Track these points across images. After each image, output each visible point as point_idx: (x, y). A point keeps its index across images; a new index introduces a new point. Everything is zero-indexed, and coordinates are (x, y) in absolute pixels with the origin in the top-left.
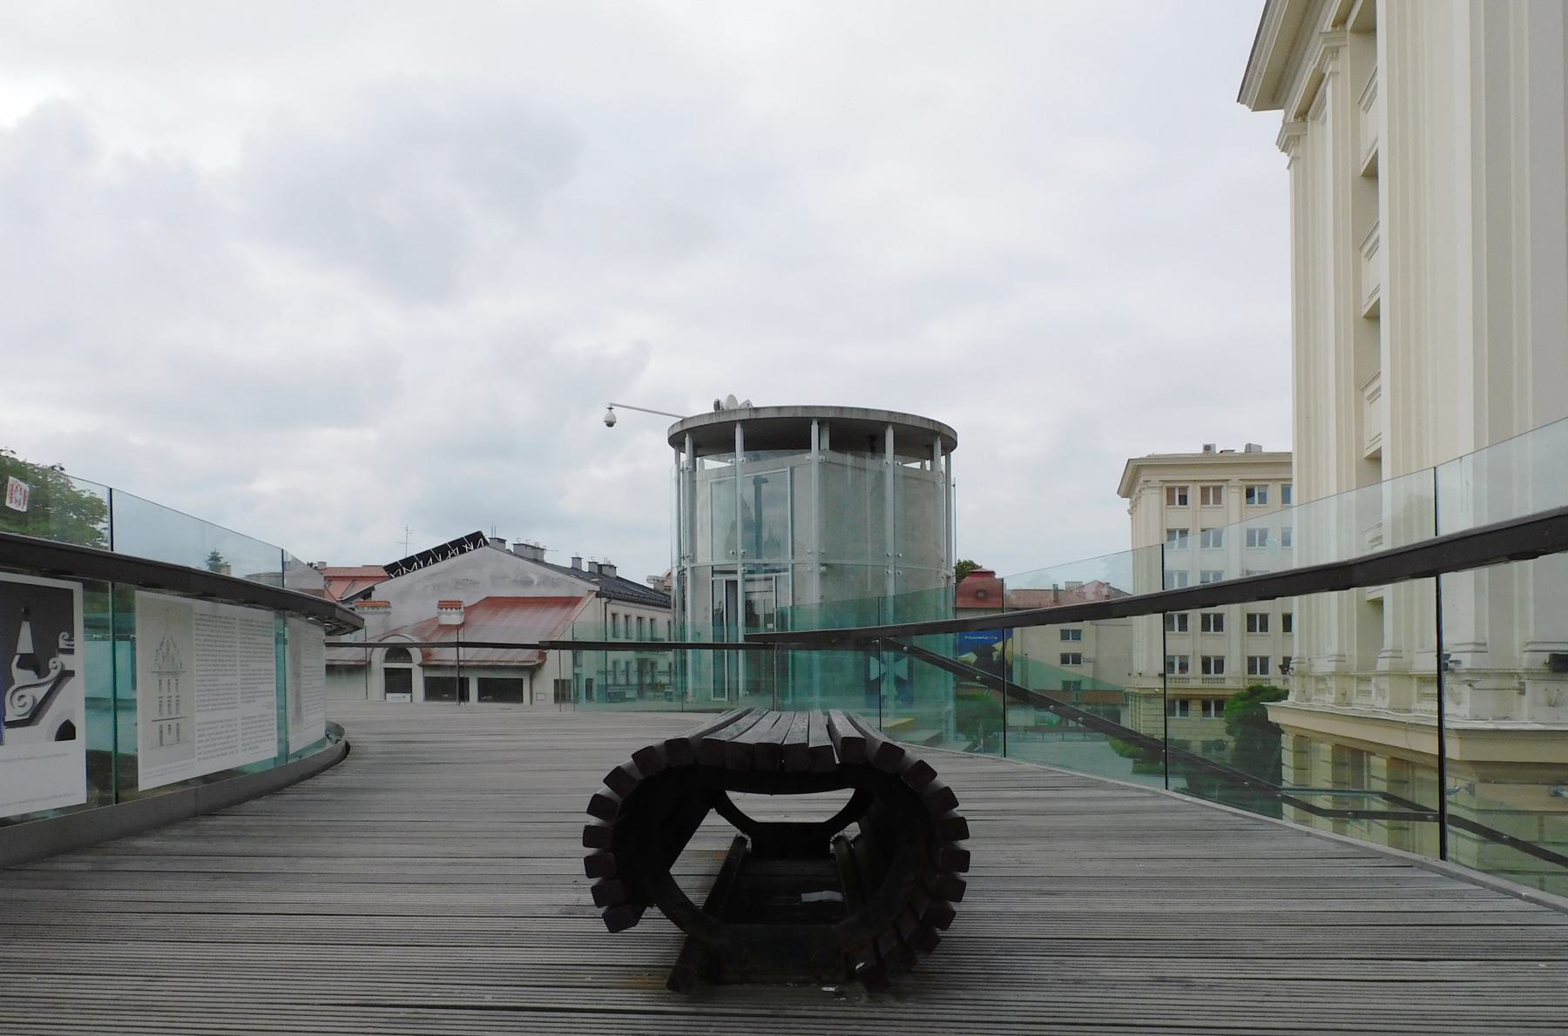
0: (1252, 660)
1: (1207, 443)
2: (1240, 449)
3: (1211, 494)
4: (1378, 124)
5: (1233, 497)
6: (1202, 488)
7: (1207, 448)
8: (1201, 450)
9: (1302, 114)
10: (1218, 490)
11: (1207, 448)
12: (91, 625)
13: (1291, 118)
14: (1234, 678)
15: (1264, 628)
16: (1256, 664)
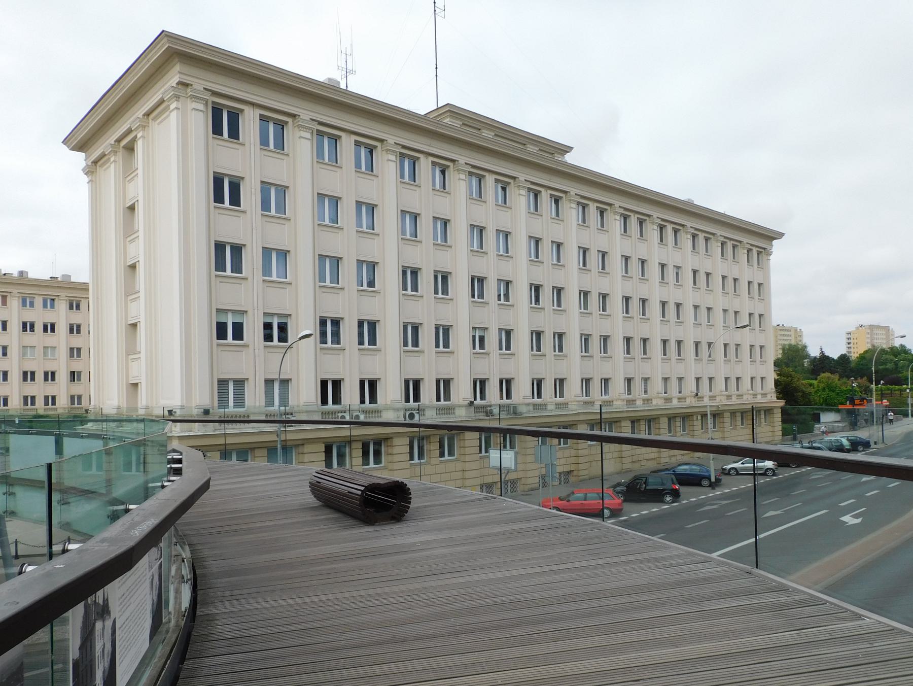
0: (25, 398)
2: (16, 274)
3: (49, 303)
4: (136, 190)
5: (62, 306)
9: (95, 162)
13: (90, 163)
15: (33, 379)
16: (29, 400)
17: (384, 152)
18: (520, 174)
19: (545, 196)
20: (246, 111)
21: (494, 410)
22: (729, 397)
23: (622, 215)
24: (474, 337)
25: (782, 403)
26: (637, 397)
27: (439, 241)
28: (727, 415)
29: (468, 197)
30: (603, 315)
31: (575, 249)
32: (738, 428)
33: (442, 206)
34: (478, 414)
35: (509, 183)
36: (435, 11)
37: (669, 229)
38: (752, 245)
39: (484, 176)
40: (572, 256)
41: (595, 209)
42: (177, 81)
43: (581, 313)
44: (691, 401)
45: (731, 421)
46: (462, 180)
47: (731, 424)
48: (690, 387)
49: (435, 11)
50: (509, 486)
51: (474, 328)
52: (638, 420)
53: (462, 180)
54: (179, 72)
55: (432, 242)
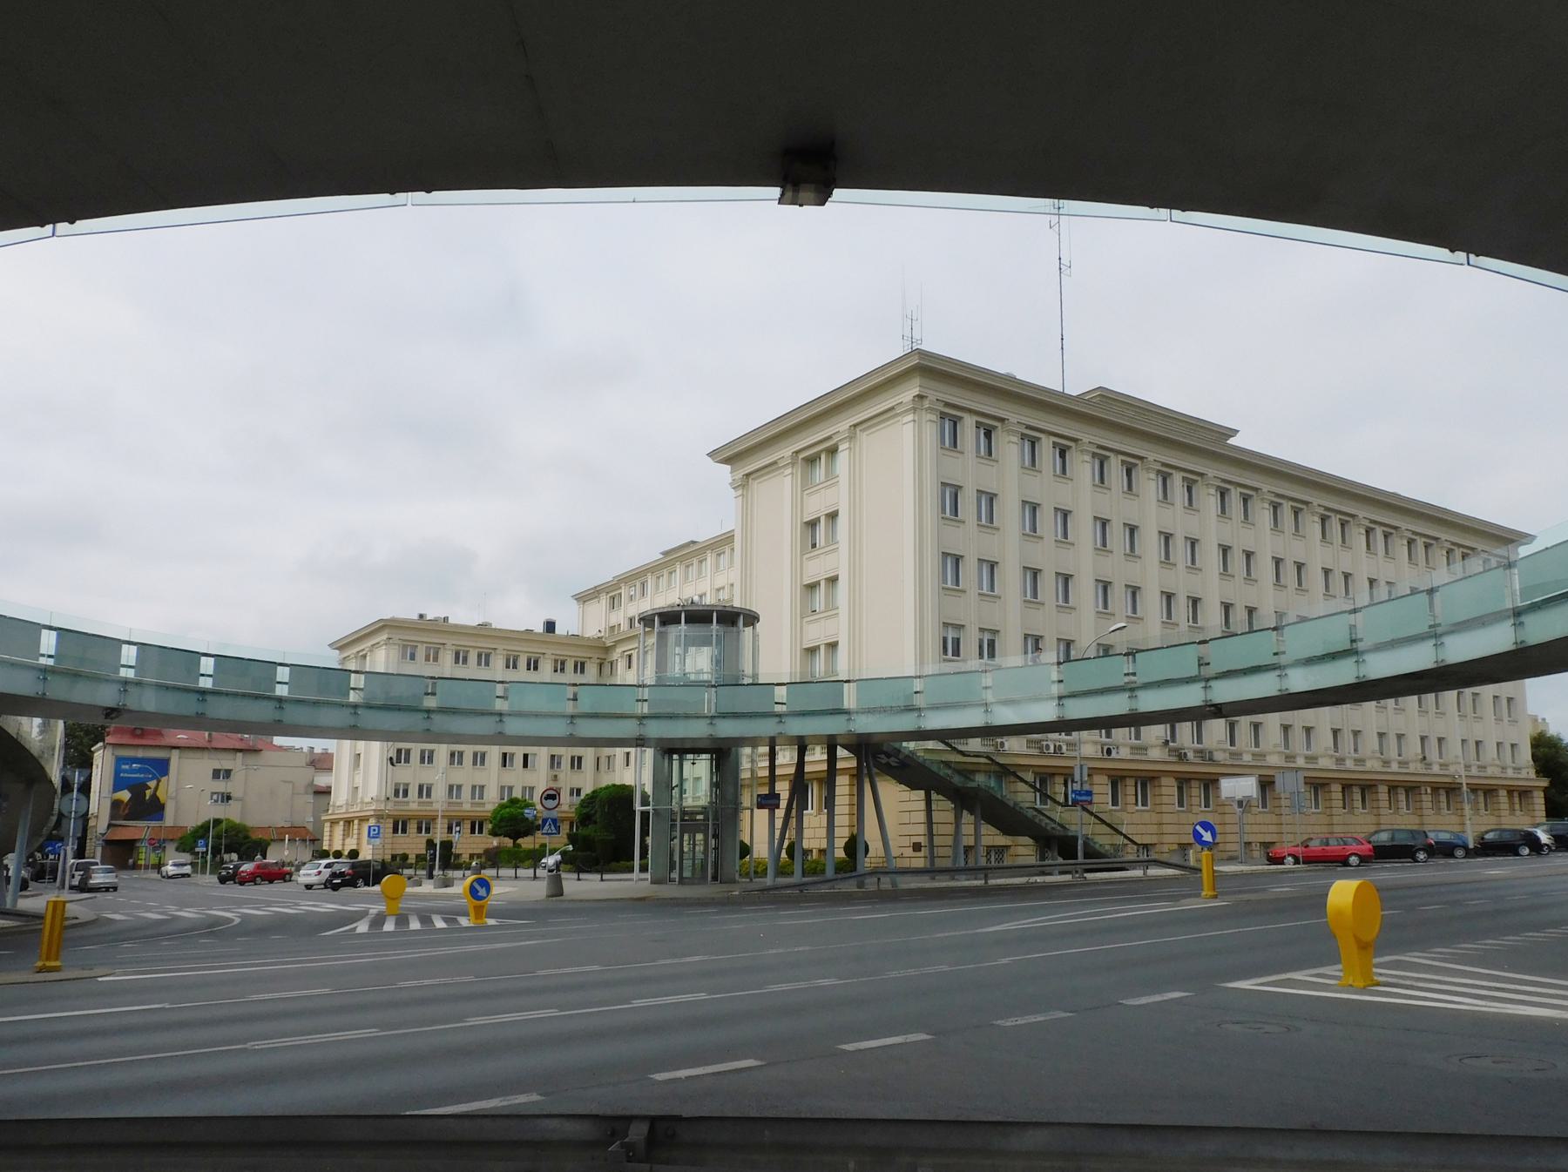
0: (451, 788)
1: (422, 612)
6: (427, 647)
7: (421, 616)
8: (416, 617)
10: (488, 656)
11: (421, 616)
12: (264, 857)
14: (492, 800)
17: (1079, 452)
18: (1149, 453)
19: (1046, 445)
20: (1043, 440)
21: (1188, 754)
22: (1340, 761)
23: (1159, 472)
24: (945, 640)
25: (1544, 783)
26: (1347, 755)
27: (984, 522)
28: (1383, 789)
29: (939, 446)
30: (1193, 627)
31: (1155, 536)
32: (1401, 812)
33: (1062, 494)
34: (1031, 750)
35: (1301, 509)
36: (1060, 269)
37: (1287, 508)
38: (1414, 533)
39: (1107, 457)
40: (1150, 543)
41: (1120, 464)
42: (917, 393)
43: (1097, 612)
44: (1415, 767)
45: (1390, 797)
46: (1013, 443)
47: (1344, 804)
48: (1413, 749)
49: (1060, 269)
50: (993, 857)
51: (946, 625)
52: (1123, 778)
53: (1013, 443)
54: (920, 386)
55: (976, 522)
